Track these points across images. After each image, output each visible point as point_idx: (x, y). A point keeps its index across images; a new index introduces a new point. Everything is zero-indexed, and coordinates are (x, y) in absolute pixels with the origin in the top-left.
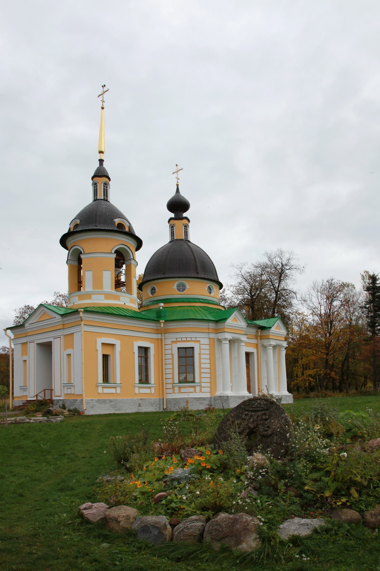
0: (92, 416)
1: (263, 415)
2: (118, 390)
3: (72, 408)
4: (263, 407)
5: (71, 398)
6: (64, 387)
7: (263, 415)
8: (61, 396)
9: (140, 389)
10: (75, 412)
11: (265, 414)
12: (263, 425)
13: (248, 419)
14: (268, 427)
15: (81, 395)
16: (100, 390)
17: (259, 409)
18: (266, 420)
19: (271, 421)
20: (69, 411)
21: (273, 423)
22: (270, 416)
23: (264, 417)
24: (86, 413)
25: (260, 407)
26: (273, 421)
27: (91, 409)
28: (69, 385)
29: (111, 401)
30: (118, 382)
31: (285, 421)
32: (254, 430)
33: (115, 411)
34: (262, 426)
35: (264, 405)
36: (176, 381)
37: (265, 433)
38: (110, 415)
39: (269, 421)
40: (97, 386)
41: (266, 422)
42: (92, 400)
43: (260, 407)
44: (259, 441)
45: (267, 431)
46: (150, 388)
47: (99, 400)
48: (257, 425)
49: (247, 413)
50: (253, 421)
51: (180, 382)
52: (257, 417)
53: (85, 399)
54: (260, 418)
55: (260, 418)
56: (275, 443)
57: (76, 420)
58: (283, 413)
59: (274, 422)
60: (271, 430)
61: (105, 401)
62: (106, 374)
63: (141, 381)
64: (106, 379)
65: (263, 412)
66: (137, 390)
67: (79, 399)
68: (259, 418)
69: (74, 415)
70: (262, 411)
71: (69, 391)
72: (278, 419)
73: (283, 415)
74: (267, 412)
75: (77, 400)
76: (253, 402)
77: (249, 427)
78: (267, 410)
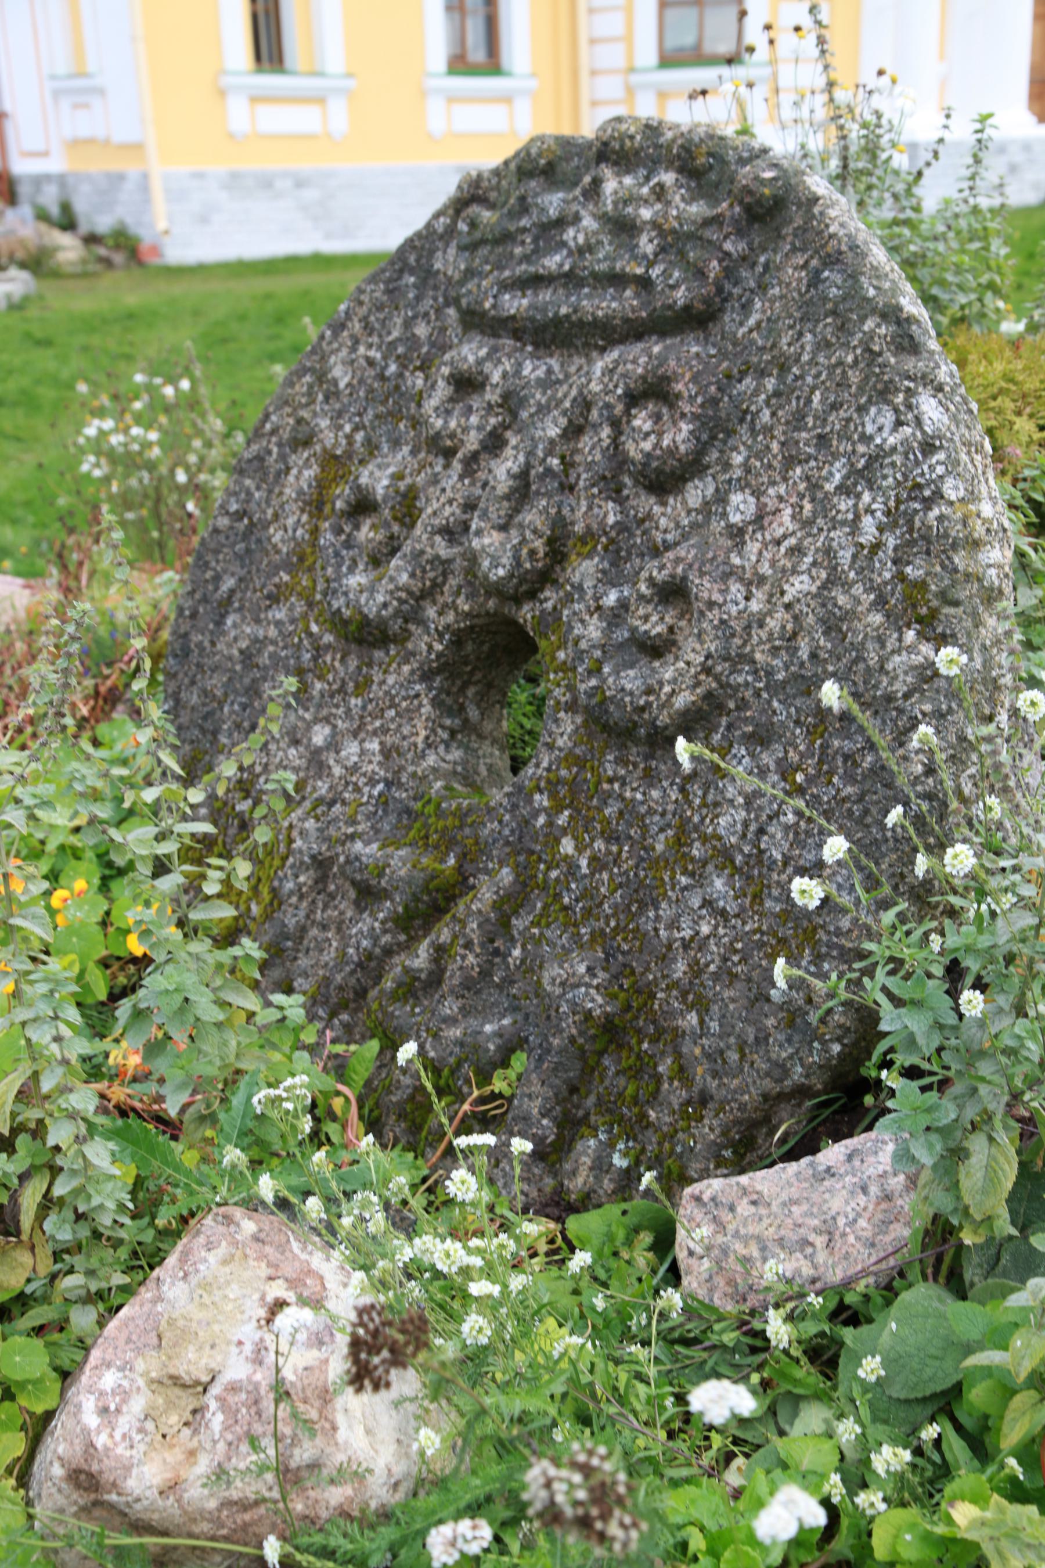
0: (200, 270)
1: (633, 399)
2: (338, 116)
3: (103, 224)
4: (644, 283)
5: (97, 165)
6: (57, 94)
7: (633, 399)
8: (45, 154)
9: (458, 109)
10: (117, 247)
11: (654, 391)
12: (619, 549)
13: (472, 441)
14: (673, 593)
15: (136, 148)
16: (238, 114)
17: (604, 305)
18: (665, 479)
19: (721, 498)
20: (92, 239)
21: (737, 534)
22: (716, 428)
23: (648, 435)
24: (176, 253)
25: (617, 280)
26: (741, 506)
27: (192, 233)
28: (78, 87)
29: (300, 183)
30: (334, 60)
31: (893, 518)
32: (526, 613)
33: (328, 236)
34: (609, 579)
35: (674, 242)
36: (647, 53)
37: (631, 680)
38: (291, 264)
39: (696, 493)
40: (222, 93)
41: (667, 516)
42: (200, 176)
43: (617, 280)
44: (552, 786)
45: (656, 649)
46: (506, 99)
47: (235, 177)
48: (559, 548)
49: (470, 352)
50: (522, 490)
51: (668, 60)
52: (574, 431)
53: (157, 170)
54: (592, 447)
55: (592, 447)
56: (724, 857)
57: (122, 292)
58: (884, 394)
59: (759, 520)
60: (692, 652)
61: (266, 183)
62: (267, 13)
63: (459, 64)
64: (268, 46)
65: (638, 358)
66: (437, 116)
67: (132, 169)
68: (586, 442)
69: (107, 263)
70: (635, 331)
71: (85, 125)
72: (814, 486)
73: (879, 424)
74: (685, 356)
75: (121, 177)
76: (553, 202)
77: (473, 579)
78: (696, 319)
